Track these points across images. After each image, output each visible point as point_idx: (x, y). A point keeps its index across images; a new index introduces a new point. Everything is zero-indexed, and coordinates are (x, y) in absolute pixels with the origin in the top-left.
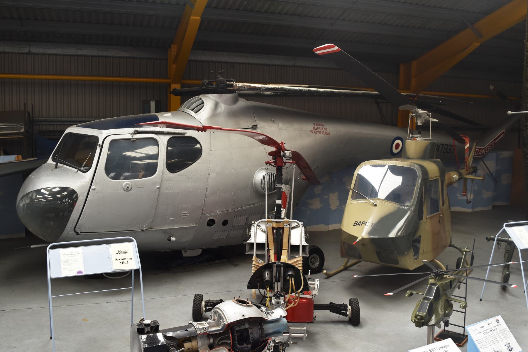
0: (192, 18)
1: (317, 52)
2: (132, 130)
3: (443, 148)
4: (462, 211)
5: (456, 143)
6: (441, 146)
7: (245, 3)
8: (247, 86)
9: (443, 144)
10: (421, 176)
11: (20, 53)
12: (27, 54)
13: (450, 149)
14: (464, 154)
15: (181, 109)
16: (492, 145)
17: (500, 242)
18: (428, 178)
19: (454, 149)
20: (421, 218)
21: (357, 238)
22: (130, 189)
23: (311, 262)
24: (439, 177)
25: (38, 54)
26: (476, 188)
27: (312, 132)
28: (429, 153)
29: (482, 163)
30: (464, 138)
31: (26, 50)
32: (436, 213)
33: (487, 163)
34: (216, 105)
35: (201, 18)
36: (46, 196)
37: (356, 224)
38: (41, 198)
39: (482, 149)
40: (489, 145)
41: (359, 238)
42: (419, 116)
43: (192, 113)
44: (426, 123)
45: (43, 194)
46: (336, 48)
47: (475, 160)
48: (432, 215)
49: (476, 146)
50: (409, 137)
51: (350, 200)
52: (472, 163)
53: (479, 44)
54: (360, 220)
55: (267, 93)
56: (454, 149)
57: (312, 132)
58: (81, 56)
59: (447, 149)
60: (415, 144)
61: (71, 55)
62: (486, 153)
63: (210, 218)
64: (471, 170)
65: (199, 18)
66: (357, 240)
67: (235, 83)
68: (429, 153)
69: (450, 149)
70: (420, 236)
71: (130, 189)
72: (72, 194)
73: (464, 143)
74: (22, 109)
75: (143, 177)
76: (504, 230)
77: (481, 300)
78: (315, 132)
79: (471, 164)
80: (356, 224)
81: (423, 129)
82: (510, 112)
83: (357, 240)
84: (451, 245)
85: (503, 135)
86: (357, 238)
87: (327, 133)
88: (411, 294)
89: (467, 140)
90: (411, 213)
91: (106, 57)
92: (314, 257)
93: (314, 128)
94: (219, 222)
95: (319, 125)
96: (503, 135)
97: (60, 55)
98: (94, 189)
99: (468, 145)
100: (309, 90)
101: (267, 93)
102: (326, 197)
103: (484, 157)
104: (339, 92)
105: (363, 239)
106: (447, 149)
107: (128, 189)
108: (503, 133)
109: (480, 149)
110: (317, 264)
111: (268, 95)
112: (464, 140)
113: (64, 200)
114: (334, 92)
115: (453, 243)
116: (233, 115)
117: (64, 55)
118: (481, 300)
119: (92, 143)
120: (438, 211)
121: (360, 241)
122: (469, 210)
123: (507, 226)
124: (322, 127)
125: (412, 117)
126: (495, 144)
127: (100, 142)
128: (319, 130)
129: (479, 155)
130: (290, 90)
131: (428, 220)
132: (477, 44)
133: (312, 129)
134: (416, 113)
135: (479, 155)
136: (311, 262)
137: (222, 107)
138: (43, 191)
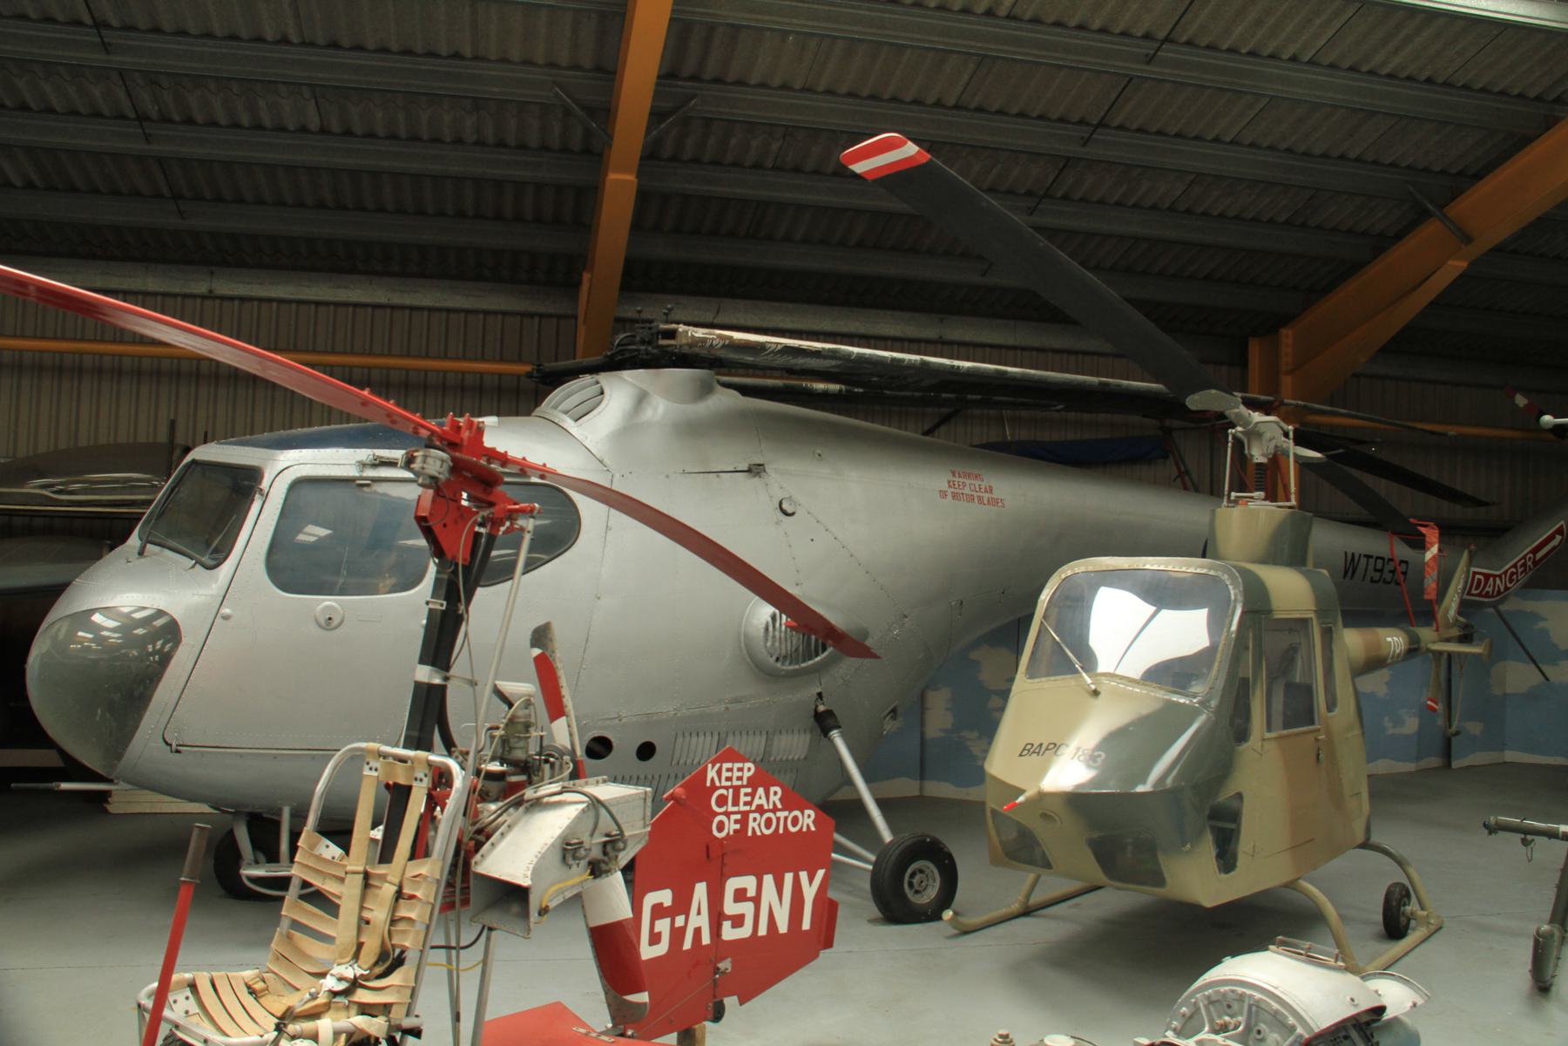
0: (612, 176)
1: (859, 168)
2: (364, 454)
3: (1371, 567)
6: (1363, 560)
7: (775, 146)
8: (720, 336)
9: (1368, 557)
10: (1240, 598)
11: (185, 296)
12: (203, 297)
14: (1423, 578)
15: (538, 411)
16: (1524, 565)
17: (1529, 837)
18: (1270, 611)
19: (1404, 573)
20: (1242, 735)
21: (1021, 791)
22: (335, 622)
23: (911, 885)
24: (1311, 615)
25: (232, 299)
30: (1423, 530)
31: (201, 288)
34: (641, 399)
35: (639, 175)
36: (105, 633)
37: (1029, 750)
38: (91, 640)
39: (1495, 576)
40: (1515, 566)
41: (1030, 793)
42: (1254, 433)
43: (568, 423)
44: (1276, 460)
45: (96, 628)
46: (911, 149)
48: (1285, 732)
49: (1470, 563)
50: (1229, 500)
52: (1459, 613)
53: (1465, 265)
54: (1056, 750)
55: (820, 386)
56: (1404, 573)
57: (943, 494)
58: (346, 304)
59: (1381, 571)
60: (1248, 519)
61: (317, 303)
62: (1507, 588)
63: (597, 733)
64: (1455, 632)
65: (631, 177)
66: (1021, 799)
67: (682, 328)
70: (1240, 796)
71: (335, 622)
72: (172, 631)
73: (1420, 544)
74: (163, 437)
75: (394, 589)
78: (955, 496)
79: (1452, 613)
80: (1029, 750)
81: (1267, 479)
82: (1547, 419)
83: (1021, 799)
85: (1558, 538)
87: (994, 502)
89: (1431, 534)
90: (1209, 719)
91: (412, 308)
92: (921, 871)
93: (951, 484)
94: (625, 745)
95: (969, 476)
96: (1558, 538)
97: (290, 302)
98: (226, 618)
100: (924, 363)
101: (820, 386)
106: (1381, 571)
107: (329, 623)
108: (1560, 531)
109: (1487, 577)
110: (932, 893)
111: (825, 395)
113: (150, 648)
114: (1005, 372)
115: (1375, 839)
116: (691, 431)
117: (300, 302)
119: (244, 483)
120: (1312, 723)
121: (1028, 801)
124: (977, 483)
125: (1236, 439)
126: (1535, 563)
127: (265, 485)
128: (967, 491)
130: (861, 357)
131: (1272, 747)
132: (1456, 266)
133: (945, 487)
134: (1246, 423)
135: (1487, 595)
136: (911, 885)
137: (660, 409)
138: (97, 618)
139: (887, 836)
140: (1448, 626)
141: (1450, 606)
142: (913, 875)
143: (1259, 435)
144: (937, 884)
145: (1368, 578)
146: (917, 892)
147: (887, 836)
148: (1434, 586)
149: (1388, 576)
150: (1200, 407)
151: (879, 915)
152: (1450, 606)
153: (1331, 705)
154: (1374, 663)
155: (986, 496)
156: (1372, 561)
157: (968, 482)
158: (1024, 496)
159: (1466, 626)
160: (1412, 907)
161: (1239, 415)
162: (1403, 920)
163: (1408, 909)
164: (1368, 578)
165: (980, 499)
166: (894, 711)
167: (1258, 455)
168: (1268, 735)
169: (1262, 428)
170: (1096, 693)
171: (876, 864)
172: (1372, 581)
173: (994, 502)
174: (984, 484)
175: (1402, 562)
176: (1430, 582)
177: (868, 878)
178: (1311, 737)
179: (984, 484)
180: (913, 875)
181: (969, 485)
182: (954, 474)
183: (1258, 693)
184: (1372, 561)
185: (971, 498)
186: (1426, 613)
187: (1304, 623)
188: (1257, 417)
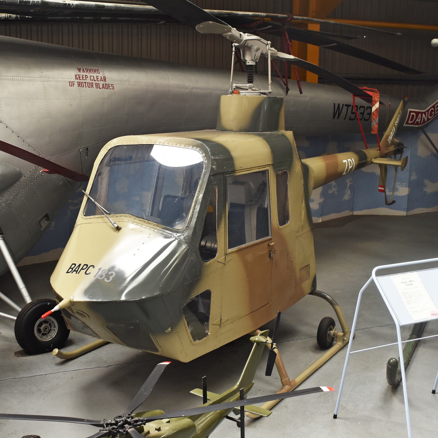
4: (397, 215)
5: (359, 101)
6: (345, 108)
9: (348, 106)
13: (363, 114)
18: (234, 171)
21: (61, 299)
26: (414, 177)
27: (72, 84)
28: (261, 121)
29: (423, 136)
32: (265, 239)
33: (431, 135)
39: (422, 113)
40: (433, 107)
42: (245, 47)
44: (264, 57)
47: (401, 130)
51: (81, 218)
62: (428, 119)
68: (261, 121)
69: (363, 114)
70: (207, 295)
73: (370, 100)
76: (373, 281)
77: (335, 417)
79: (390, 138)
81: (252, 73)
84: (313, 292)
86: (61, 299)
87: (106, 86)
88: (169, 422)
89: (376, 97)
99: (377, 105)
102: (137, 199)
103: (427, 126)
104: (117, 9)
105: (72, 303)
109: (417, 113)
112: (371, 97)
114: (103, 7)
118: (335, 417)
122: (403, 213)
123: (378, 273)
124: (95, 75)
128: (88, 80)
129: (417, 123)
134: (238, 41)
135: (417, 123)
136: (39, 331)
139: (28, 300)
140: (387, 145)
141: (390, 133)
142: (40, 325)
143: (250, 48)
144: (57, 329)
145: (348, 117)
146: (44, 334)
147: (28, 300)
148: (376, 126)
149: (360, 116)
150: (205, 32)
151: (21, 349)
152: (390, 133)
153: (284, 218)
154: (334, 176)
155: (101, 83)
156: (350, 108)
157: (89, 75)
158: (126, 81)
159: (399, 144)
160: (337, 331)
161: (232, 36)
162: (329, 340)
163: (332, 332)
164: (348, 117)
165: (97, 86)
166: (47, 216)
167: (249, 60)
168: (230, 250)
169: (250, 43)
170: (118, 229)
171: (20, 316)
172: (350, 119)
173: (106, 86)
174: (100, 75)
175: (361, 107)
176: (375, 124)
177: (13, 324)
178: (266, 244)
179: (100, 75)
180: (40, 325)
181: (90, 76)
182: (79, 70)
183: (222, 225)
184: (350, 108)
185: (91, 85)
186: (375, 139)
187: (264, 173)
188: (246, 37)
